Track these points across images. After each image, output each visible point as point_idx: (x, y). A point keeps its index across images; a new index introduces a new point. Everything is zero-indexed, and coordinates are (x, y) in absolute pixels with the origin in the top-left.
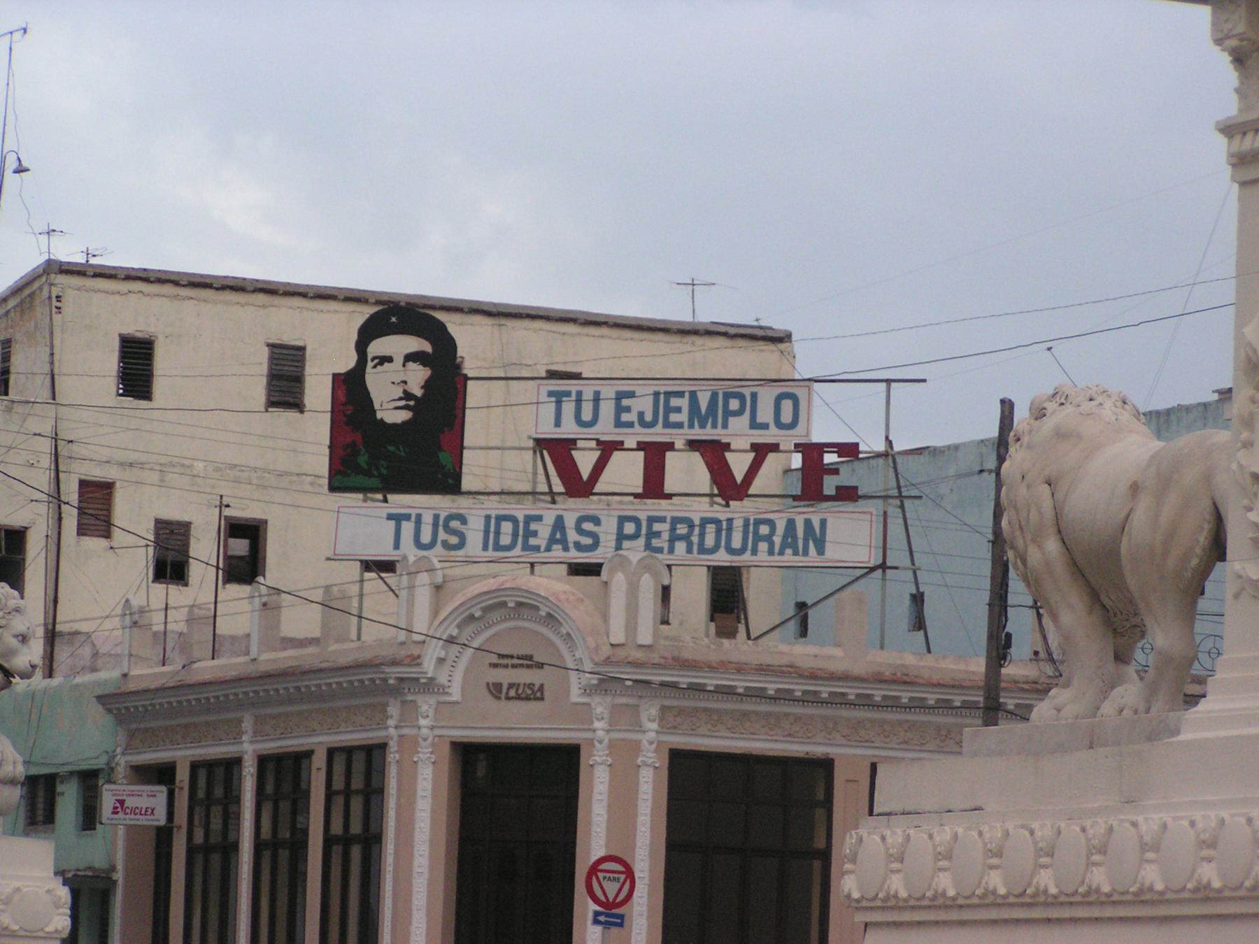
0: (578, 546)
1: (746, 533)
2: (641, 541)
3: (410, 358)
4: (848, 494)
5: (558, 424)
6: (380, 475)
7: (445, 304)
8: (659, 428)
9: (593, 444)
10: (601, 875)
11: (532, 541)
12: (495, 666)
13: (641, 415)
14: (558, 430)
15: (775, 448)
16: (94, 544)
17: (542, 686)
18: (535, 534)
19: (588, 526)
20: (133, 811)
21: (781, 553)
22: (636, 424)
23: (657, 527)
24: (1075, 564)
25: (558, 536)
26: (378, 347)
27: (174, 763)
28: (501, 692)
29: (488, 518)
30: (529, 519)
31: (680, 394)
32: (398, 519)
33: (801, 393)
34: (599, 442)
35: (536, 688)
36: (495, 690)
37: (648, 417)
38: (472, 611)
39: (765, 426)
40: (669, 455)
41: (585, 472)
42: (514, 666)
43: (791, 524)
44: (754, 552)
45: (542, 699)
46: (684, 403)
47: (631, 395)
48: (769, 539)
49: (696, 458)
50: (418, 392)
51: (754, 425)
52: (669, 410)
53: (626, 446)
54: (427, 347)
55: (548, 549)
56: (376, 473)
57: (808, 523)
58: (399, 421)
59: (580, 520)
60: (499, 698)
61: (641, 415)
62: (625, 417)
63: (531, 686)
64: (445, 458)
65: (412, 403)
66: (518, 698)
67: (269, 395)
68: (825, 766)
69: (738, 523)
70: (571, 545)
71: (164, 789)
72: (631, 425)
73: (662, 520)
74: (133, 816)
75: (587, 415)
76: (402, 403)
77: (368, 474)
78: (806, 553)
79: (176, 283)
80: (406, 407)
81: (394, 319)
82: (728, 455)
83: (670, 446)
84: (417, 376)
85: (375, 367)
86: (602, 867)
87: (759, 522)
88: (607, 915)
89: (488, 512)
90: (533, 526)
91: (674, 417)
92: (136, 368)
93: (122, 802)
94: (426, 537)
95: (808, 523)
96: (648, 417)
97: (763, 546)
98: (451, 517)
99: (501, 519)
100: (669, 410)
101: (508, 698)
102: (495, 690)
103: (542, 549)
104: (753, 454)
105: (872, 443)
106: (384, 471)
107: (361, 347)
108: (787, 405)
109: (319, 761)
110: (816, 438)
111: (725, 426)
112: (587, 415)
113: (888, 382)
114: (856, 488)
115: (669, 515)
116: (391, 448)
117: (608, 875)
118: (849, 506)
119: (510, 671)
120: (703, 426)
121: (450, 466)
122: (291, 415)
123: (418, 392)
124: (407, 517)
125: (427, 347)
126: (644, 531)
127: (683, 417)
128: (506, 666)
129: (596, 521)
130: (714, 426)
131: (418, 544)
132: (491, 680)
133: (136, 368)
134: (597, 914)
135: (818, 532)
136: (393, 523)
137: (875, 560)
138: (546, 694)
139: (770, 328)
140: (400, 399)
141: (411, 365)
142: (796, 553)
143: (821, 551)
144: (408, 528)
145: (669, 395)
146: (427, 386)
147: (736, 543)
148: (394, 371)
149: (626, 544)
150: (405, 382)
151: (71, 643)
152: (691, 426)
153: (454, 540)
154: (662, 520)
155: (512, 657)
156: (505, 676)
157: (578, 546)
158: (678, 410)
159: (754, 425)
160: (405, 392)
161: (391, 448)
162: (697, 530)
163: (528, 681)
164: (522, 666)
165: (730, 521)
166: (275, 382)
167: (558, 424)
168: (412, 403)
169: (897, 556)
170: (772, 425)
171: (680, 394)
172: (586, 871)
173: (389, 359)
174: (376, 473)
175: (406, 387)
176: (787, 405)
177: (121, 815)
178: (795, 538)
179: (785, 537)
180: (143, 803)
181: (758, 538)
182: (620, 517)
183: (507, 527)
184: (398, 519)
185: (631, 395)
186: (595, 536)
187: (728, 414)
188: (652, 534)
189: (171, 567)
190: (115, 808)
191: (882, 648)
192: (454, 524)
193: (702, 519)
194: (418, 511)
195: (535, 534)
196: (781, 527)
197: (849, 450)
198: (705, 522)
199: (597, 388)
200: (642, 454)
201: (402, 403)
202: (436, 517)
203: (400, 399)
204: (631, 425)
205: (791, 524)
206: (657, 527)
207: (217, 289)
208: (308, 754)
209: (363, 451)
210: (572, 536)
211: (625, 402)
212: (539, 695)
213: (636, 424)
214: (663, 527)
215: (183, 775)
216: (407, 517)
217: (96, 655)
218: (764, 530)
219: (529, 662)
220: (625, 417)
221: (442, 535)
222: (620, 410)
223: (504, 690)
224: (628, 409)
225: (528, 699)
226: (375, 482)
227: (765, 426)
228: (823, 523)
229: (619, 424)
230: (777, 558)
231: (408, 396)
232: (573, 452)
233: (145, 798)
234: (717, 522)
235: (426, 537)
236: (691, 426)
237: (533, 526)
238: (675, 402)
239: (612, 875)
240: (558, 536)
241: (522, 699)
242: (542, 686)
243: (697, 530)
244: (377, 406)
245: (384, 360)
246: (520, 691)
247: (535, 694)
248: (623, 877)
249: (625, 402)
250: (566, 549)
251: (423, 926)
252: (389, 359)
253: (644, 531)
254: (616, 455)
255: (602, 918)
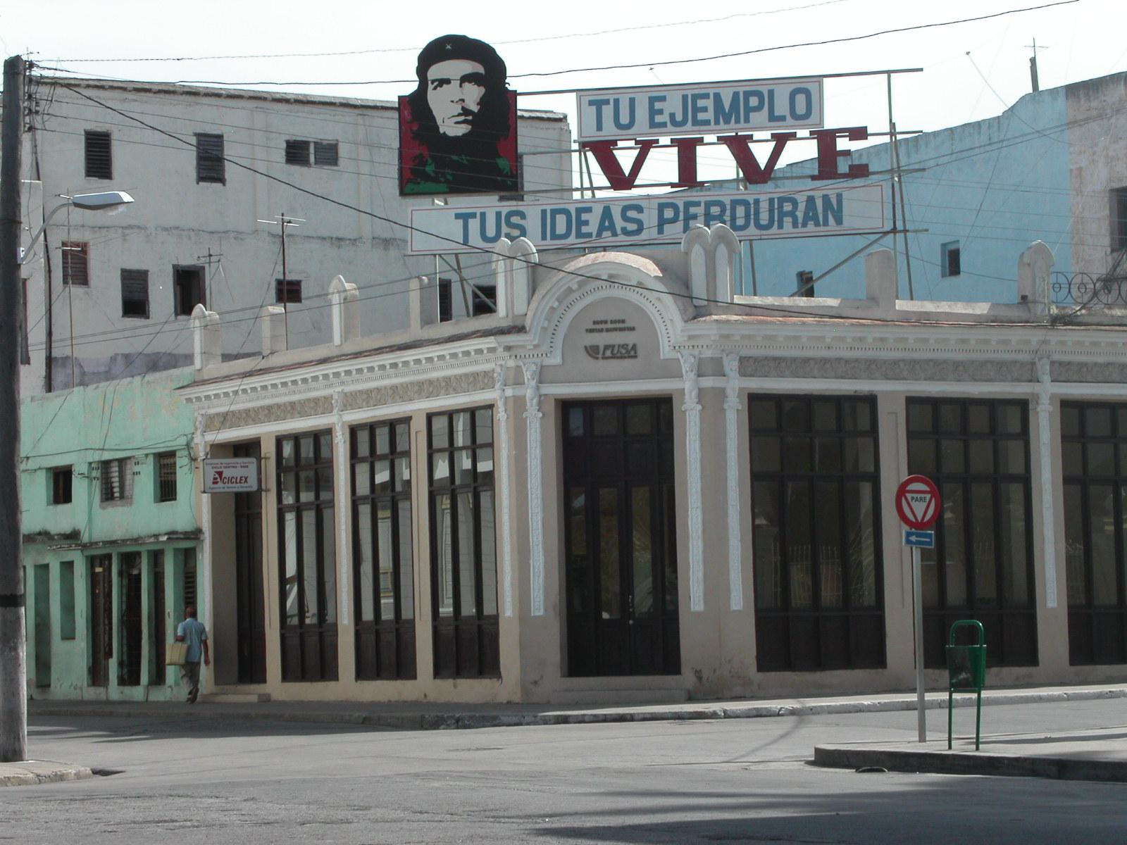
0: (626, 232)
1: (771, 211)
2: (680, 225)
3: (465, 79)
4: (859, 171)
5: (599, 128)
6: (447, 181)
7: (322, 100)
8: (689, 126)
9: (632, 143)
10: (909, 496)
11: (585, 229)
12: (591, 331)
13: (672, 116)
14: (599, 133)
15: (793, 136)
16: (77, 290)
17: (634, 346)
18: (586, 223)
19: (632, 214)
20: (230, 480)
21: (805, 225)
22: (669, 124)
23: (693, 210)
24: (679, 295)
25: (607, 224)
26: (435, 72)
27: (260, 438)
28: (598, 353)
29: (544, 212)
30: (580, 211)
31: (706, 96)
32: (465, 217)
33: (812, 87)
34: (637, 142)
35: (630, 347)
36: (593, 351)
37: (679, 118)
38: (570, 284)
39: (783, 118)
40: (700, 149)
41: (627, 168)
42: (608, 330)
43: (811, 200)
44: (780, 226)
45: (635, 357)
46: (709, 103)
47: (663, 99)
48: (792, 214)
49: (724, 150)
50: (475, 109)
51: (773, 118)
52: (696, 110)
53: (661, 143)
54: (480, 69)
55: (599, 235)
56: (442, 180)
57: (826, 198)
58: (460, 134)
59: (625, 209)
60: (597, 358)
61: (672, 116)
62: (658, 119)
63: (624, 346)
64: (503, 163)
65: (470, 118)
66: (614, 357)
67: (199, 173)
68: (870, 401)
69: (764, 206)
70: (619, 231)
71: (254, 460)
72: (664, 125)
73: (698, 204)
74: (230, 485)
75: (624, 119)
76: (462, 118)
77: (436, 180)
78: (826, 223)
79: (124, 89)
80: (464, 122)
81: (449, 47)
82: (751, 145)
83: (700, 141)
84: (473, 95)
85: (435, 88)
86: (910, 487)
87: (782, 200)
88: (918, 535)
89: (544, 207)
90: (584, 217)
91: (701, 116)
92: (98, 153)
93: (220, 474)
94: (491, 232)
95: (826, 198)
96: (679, 118)
97: (788, 221)
98: (510, 214)
99: (555, 212)
100: (696, 110)
101: (604, 358)
102: (593, 351)
103: (594, 235)
104: (773, 143)
105: (878, 124)
106: (450, 178)
107: (422, 70)
108: (801, 98)
109: (419, 425)
110: (829, 124)
111: (747, 120)
112: (624, 119)
113: (889, 72)
114: (867, 166)
115: (703, 200)
116: (455, 157)
117: (915, 495)
118: (858, 182)
119: (604, 334)
120: (727, 122)
121: (507, 170)
122: (217, 186)
123: (475, 109)
124: (473, 215)
125: (480, 69)
126: (681, 217)
127: (709, 115)
128: (601, 330)
129: (639, 209)
130: (738, 121)
131: (485, 238)
132: (588, 344)
133: (98, 153)
134: (909, 535)
135: (835, 207)
136: (461, 222)
137: (888, 226)
138: (639, 353)
139: (552, 112)
140: (459, 115)
141: (466, 85)
142: (817, 224)
143: (839, 221)
144: (474, 225)
145: (695, 97)
146: (482, 102)
147: (764, 218)
148: (452, 91)
149: (666, 227)
150: (463, 100)
151: (64, 366)
152: (717, 122)
153: (632, 227)
154: (698, 204)
155: (606, 322)
156: (601, 340)
157: (626, 232)
158: (705, 109)
159: (773, 118)
160: (463, 108)
161: (455, 157)
162: (728, 213)
163: (622, 342)
164: (615, 329)
165: (757, 202)
166: (202, 163)
167: (599, 128)
168: (470, 118)
169: (900, 226)
170: (788, 117)
171: (706, 96)
172: (895, 490)
173: (448, 81)
174: (442, 180)
175: (463, 104)
176: (801, 98)
177: (220, 484)
178: (816, 215)
179: (806, 214)
180: (237, 473)
181: (782, 214)
182: (660, 205)
183: (561, 220)
184: (465, 217)
185: (663, 99)
186: (640, 223)
187: (749, 110)
188: (689, 218)
189: (135, 305)
190: (215, 479)
191: (912, 299)
192: (515, 220)
193: (731, 201)
194: (483, 210)
195: (586, 223)
196: (802, 207)
197: (859, 133)
198: (735, 203)
199: (632, 96)
200: (676, 149)
201: (462, 118)
202: (498, 214)
203: (459, 115)
204: (664, 125)
205: (811, 200)
206: (693, 210)
207: (155, 93)
208: (407, 420)
209: (430, 161)
210: (619, 223)
211: (658, 105)
212: (632, 353)
213: (669, 124)
214: (700, 210)
215: (268, 449)
216: (473, 215)
217: (83, 374)
218: (788, 207)
219: (620, 326)
220: (658, 119)
221: (505, 229)
222: (653, 112)
223: (601, 350)
224: (661, 112)
225: (622, 357)
226: (443, 187)
227: (783, 118)
228: (839, 196)
229: (653, 124)
230: (822, 228)
231: (466, 112)
232: (615, 152)
233: (239, 469)
234: (745, 203)
235: (491, 232)
236: (717, 122)
237: (584, 217)
238: (701, 103)
239: (919, 496)
240: (607, 224)
241: (618, 358)
242: (634, 346)
243: (728, 213)
244: (439, 122)
245: (443, 82)
246: (615, 351)
247: (629, 352)
248: (928, 496)
249: (658, 105)
250: (615, 234)
251: (542, 559)
252: (448, 81)
253: (681, 217)
254: (653, 153)
255: (913, 538)
